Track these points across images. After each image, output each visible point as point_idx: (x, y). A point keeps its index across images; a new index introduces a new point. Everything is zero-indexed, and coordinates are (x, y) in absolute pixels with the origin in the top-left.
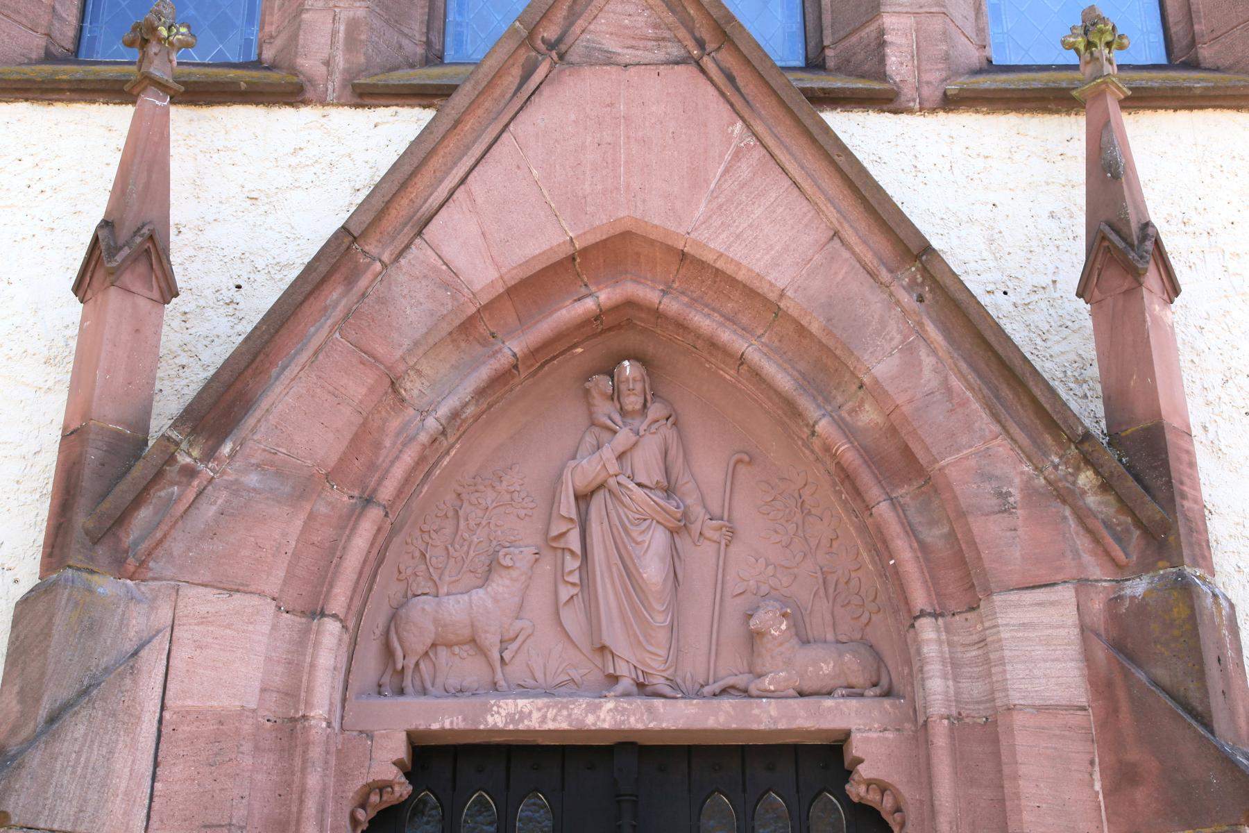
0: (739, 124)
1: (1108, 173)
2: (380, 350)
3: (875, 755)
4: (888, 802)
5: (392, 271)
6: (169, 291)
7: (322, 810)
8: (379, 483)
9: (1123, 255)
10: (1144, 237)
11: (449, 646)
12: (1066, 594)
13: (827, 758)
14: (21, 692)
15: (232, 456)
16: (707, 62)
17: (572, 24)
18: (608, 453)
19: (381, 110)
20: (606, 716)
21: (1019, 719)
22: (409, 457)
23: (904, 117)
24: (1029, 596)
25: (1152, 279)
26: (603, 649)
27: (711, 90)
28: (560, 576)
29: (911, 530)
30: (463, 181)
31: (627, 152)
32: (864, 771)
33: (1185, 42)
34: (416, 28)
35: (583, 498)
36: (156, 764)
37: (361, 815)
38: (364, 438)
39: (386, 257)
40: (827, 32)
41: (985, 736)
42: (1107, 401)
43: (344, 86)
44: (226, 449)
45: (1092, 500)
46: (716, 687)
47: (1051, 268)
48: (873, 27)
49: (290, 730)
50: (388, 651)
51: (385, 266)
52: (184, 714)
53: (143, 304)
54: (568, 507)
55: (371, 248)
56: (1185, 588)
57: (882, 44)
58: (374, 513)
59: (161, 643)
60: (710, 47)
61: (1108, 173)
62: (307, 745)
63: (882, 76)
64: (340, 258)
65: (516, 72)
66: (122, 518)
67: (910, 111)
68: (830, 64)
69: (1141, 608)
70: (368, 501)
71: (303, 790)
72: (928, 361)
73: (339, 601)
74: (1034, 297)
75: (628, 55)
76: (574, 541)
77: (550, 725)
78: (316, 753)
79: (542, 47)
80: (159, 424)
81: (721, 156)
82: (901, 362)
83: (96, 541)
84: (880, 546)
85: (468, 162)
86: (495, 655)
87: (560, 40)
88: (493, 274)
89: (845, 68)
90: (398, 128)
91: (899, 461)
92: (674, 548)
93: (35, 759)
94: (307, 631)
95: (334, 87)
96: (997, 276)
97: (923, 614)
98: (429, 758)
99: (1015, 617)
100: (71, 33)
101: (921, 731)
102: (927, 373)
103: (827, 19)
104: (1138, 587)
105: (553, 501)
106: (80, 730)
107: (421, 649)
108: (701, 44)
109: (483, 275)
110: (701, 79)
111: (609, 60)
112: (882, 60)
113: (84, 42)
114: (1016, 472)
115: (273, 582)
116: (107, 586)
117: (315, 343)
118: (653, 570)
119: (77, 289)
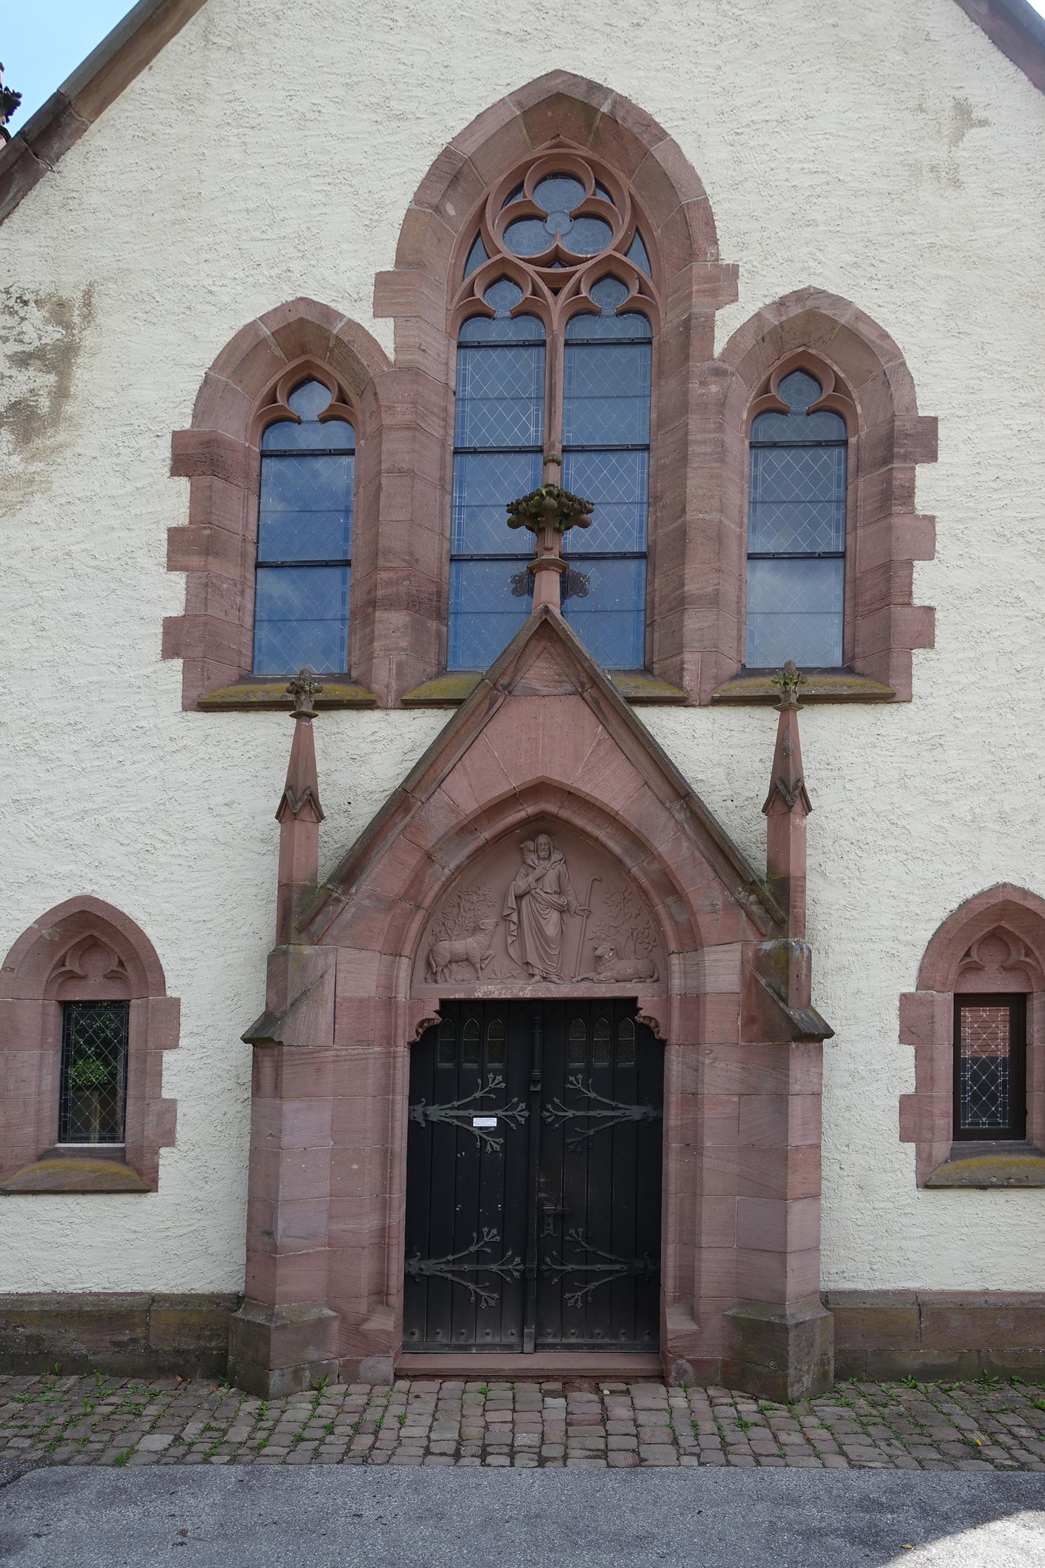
0: (601, 727)
1: (786, 753)
2: (422, 843)
3: (648, 1006)
4: (652, 1025)
5: (427, 805)
6: (320, 817)
7: (404, 1031)
8: (424, 898)
9: (787, 795)
10: (796, 787)
11: (457, 962)
12: (737, 947)
13: (630, 1004)
14: (277, 992)
15: (357, 891)
16: (585, 694)
17: (516, 675)
18: (531, 878)
19: (416, 711)
20: (528, 991)
21: (708, 998)
22: (436, 887)
23: (691, 710)
24: (720, 948)
25: (798, 807)
26: (527, 963)
27: (587, 708)
28: (508, 933)
29: (671, 916)
30: (460, 759)
31: (543, 738)
32: (642, 1013)
33: (851, 655)
34: (432, 657)
35: (519, 898)
36: (335, 1018)
37: (421, 1031)
38: (417, 879)
39: (423, 800)
40: (656, 654)
41: (694, 1003)
42: (769, 862)
43: (396, 699)
44: (353, 890)
45: (755, 908)
46: (579, 978)
47: (757, 788)
48: (678, 658)
49: (389, 1003)
50: (429, 964)
51: (423, 803)
52: (345, 999)
53: (310, 825)
54: (512, 902)
55: (417, 795)
56: (787, 948)
57: (682, 669)
58: (422, 912)
59: (331, 971)
60: (587, 686)
61: (786, 753)
62: (397, 1008)
63: (680, 687)
64: (401, 802)
65: (487, 702)
66: (312, 921)
67: (694, 706)
68: (656, 672)
69: (768, 954)
70: (418, 907)
71: (396, 1025)
72: (685, 844)
73: (408, 949)
74: (746, 803)
75: (545, 691)
76: (514, 917)
77: (503, 996)
78: (401, 1011)
79: (500, 688)
80: (321, 880)
81: (591, 744)
82: (672, 844)
83: (300, 932)
84: (657, 921)
85: (462, 750)
86: (478, 966)
87: (509, 684)
88: (475, 806)
89: (664, 677)
90: (424, 727)
91: (669, 886)
92: (562, 919)
93: (289, 1021)
94: (394, 962)
95: (391, 700)
96: (729, 793)
97: (673, 953)
98: (447, 1006)
99: (713, 957)
100: (249, 662)
101: (668, 1000)
102: (684, 850)
103: (656, 647)
104: (768, 945)
105: (505, 899)
106: (304, 1009)
107: (443, 964)
108: (582, 685)
109: (470, 806)
110: (582, 703)
111: (535, 693)
112: (682, 678)
113: (256, 665)
114: (718, 895)
115: (379, 946)
116: (307, 950)
117: (391, 840)
118: (551, 929)
119: (277, 817)
